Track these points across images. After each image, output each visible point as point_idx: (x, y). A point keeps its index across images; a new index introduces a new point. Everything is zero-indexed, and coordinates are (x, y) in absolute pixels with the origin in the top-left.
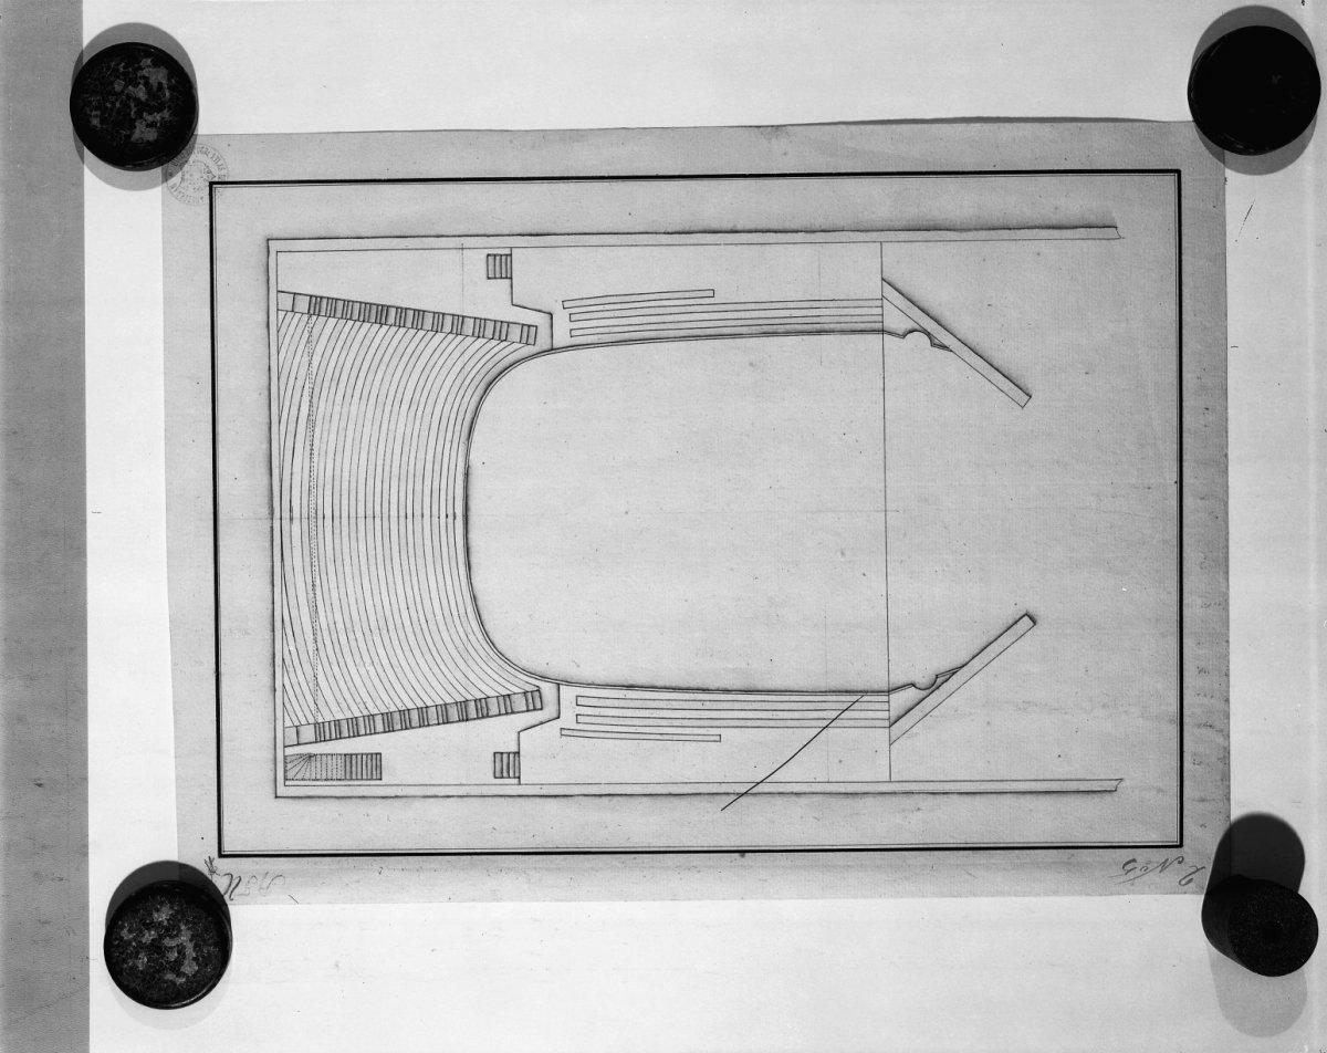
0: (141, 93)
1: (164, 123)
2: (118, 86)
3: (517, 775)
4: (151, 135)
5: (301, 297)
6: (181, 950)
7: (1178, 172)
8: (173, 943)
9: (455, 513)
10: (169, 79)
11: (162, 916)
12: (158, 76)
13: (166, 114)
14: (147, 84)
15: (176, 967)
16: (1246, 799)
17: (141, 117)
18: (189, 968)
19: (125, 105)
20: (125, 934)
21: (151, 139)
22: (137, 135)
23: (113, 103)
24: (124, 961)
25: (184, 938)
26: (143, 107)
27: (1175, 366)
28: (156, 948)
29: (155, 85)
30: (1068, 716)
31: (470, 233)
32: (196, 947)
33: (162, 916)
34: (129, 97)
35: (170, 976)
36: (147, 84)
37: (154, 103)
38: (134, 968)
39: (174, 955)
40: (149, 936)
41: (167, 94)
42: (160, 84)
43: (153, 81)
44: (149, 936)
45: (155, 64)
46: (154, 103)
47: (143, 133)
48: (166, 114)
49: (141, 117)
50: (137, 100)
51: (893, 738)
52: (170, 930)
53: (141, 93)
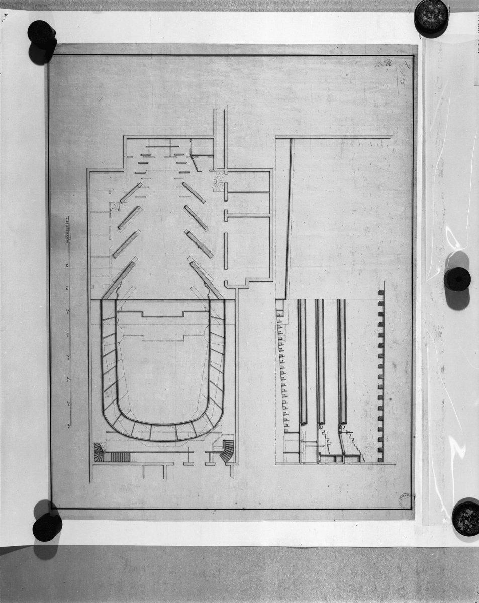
1: (464, 512)
2: (471, 526)
4: (468, 511)
5: (212, 159)
6: (429, 18)
8: (432, 17)
10: (458, 523)
11: (440, 17)
12: (460, 524)
13: (462, 514)
14: (464, 523)
15: (426, 15)
16: (42, 69)
18: (425, 18)
19: (471, 520)
20: (439, 6)
22: (472, 512)
24: (433, 2)
25: (432, 20)
26: (467, 518)
28: (433, 12)
30: (75, 74)
32: (429, 22)
33: (440, 17)
35: (424, 13)
36: (464, 523)
38: (430, 4)
39: (429, 15)
40: (437, 11)
43: (462, 524)
44: (437, 11)
45: (460, 528)
47: (470, 512)
48: (462, 514)
50: (468, 520)
52: (436, 17)
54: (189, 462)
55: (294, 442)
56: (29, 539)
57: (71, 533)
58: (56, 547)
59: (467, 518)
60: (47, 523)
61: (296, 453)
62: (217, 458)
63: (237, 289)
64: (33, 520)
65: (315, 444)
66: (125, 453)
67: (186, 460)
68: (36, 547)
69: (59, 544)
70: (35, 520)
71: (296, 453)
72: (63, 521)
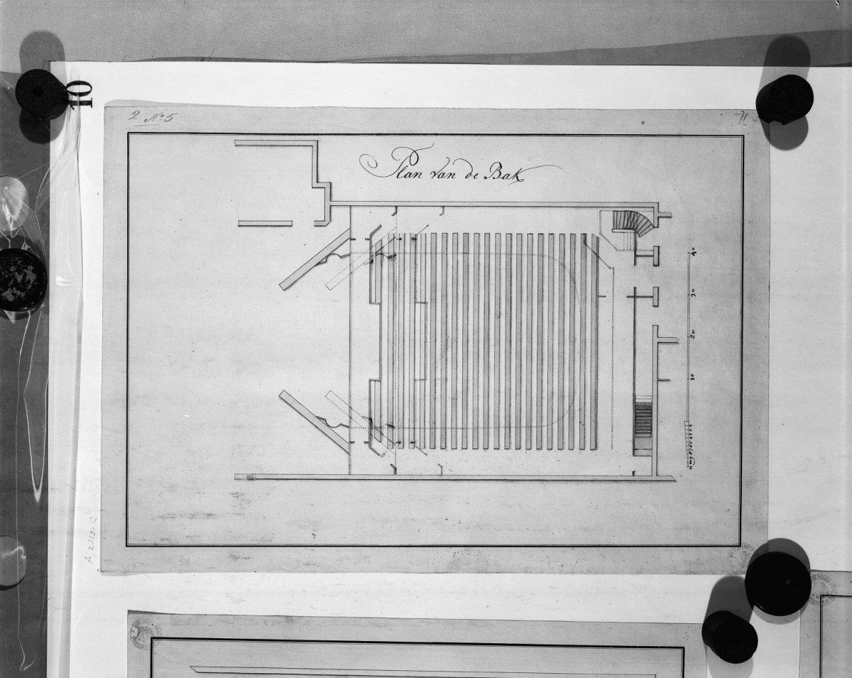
0: (19, 278)
1: (19, 297)
3: (423, 301)
7: (743, 136)
9: (553, 392)
10: (35, 281)
12: (32, 277)
13: (23, 294)
14: (24, 277)
17: (12, 288)
19: (9, 279)
21: (9, 300)
22: (4, 294)
23: (5, 274)
26: (16, 285)
27: (585, 543)
29: (27, 280)
31: (690, 543)
34: (14, 276)
36: (24, 277)
37: (21, 286)
41: (30, 287)
42: (30, 280)
43: (28, 277)
46: (21, 286)
48: (23, 294)
49: (12, 288)
50: (16, 280)
51: (349, 231)
53: (19, 278)
54: (653, 256)
55: (613, 243)
56: (816, 77)
57: (743, 85)
58: (770, 61)
59: (16, 285)
60: (784, 108)
61: (639, 297)
62: (646, 243)
63: (333, 203)
64: (809, 116)
65: (638, 253)
66: (637, 407)
67: (650, 301)
68: (806, 62)
69: (762, 68)
70: (808, 116)
71: (639, 297)
72: (754, 107)
